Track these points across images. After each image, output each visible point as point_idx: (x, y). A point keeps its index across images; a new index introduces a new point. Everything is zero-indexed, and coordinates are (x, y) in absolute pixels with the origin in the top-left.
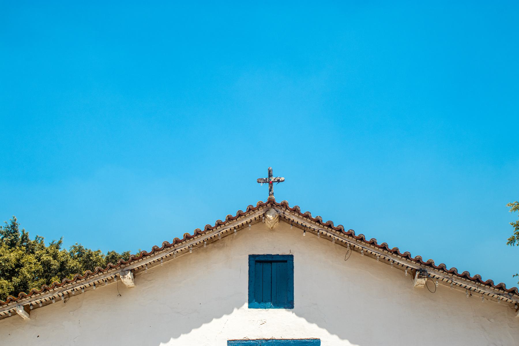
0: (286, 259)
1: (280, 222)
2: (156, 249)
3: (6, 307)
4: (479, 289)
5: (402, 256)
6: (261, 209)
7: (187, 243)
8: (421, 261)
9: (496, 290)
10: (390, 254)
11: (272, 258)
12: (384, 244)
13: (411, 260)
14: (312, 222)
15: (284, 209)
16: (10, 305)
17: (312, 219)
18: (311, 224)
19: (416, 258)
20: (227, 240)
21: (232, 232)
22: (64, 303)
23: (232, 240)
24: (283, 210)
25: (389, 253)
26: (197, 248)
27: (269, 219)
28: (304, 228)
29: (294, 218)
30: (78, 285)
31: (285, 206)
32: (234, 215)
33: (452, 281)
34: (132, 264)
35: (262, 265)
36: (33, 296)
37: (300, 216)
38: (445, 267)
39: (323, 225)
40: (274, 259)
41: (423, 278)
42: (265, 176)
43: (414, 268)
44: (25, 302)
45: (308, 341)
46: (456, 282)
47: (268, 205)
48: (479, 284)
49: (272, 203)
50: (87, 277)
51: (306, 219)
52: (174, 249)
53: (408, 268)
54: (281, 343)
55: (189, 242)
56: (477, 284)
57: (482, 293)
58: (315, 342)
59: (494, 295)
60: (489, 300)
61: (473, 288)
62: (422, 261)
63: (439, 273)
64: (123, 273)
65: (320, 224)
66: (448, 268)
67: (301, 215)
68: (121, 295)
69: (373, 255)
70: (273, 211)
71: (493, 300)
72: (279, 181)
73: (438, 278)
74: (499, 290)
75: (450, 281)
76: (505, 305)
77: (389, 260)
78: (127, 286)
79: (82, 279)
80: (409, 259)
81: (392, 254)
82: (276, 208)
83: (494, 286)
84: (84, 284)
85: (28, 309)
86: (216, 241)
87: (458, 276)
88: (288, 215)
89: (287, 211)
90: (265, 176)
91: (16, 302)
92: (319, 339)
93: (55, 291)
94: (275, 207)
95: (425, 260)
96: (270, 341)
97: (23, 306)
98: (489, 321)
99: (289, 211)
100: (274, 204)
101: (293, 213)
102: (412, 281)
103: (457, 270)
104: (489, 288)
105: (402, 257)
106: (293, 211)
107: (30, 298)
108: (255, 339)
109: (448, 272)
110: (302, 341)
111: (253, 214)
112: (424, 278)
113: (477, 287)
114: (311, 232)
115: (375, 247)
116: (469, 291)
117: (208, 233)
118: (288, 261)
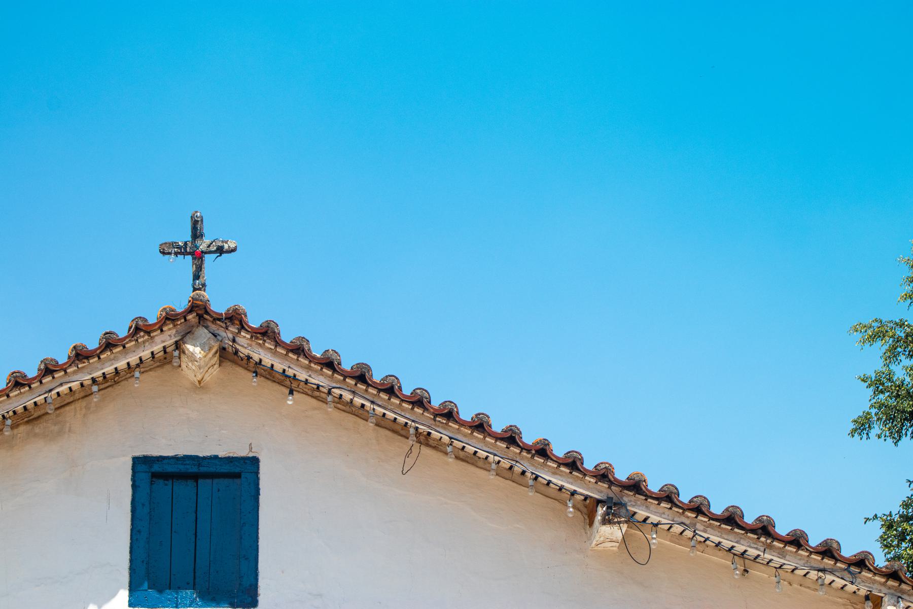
0: (237, 470)
1: (224, 364)
4: (768, 556)
5: (560, 463)
6: (170, 329)
8: (610, 477)
10: (527, 457)
12: (511, 430)
13: (585, 475)
14: (312, 365)
15: (233, 329)
17: (312, 359)
19: (598, 467)
21: (85, 392)
24: (232, 332)
25: (524, 454)
28: (290, 384)
37: (279, 350)
38: (675, 494)
39: (342, 375)
40: (203, 469)
41: (615, 523)
42: (184, 236)
46: (706, 535)
47: (190, 317)
48: (769, 541)
51: (295, 357)
56: (763, 543)
59: (808, 573)
60: (795, 586)
61: (752, 552)
62: (614, 477)
63: (661, 511)
65: (334, 370)
67: (283, 347)
69: (479, 458)
71: (805, 587)
75: (689, 533)
80: (578, 470)
82: (213, 327)
87: (711, 519)
88: (246, 346)
90: (184, 236)
94: (210, 324)
95: (621, 475)
99: (248, 336)
100: (205, 316)
101: (261, 342)
104: (796, 552)
105: (560, 465)
109: (685, 508)
111: (147, 344)
112: (619, 523)
113: (762, 549)
114: (310, 392)
115: (485, 437)
116: (741, 561)
117: (16, 396)
118: (243, 476)
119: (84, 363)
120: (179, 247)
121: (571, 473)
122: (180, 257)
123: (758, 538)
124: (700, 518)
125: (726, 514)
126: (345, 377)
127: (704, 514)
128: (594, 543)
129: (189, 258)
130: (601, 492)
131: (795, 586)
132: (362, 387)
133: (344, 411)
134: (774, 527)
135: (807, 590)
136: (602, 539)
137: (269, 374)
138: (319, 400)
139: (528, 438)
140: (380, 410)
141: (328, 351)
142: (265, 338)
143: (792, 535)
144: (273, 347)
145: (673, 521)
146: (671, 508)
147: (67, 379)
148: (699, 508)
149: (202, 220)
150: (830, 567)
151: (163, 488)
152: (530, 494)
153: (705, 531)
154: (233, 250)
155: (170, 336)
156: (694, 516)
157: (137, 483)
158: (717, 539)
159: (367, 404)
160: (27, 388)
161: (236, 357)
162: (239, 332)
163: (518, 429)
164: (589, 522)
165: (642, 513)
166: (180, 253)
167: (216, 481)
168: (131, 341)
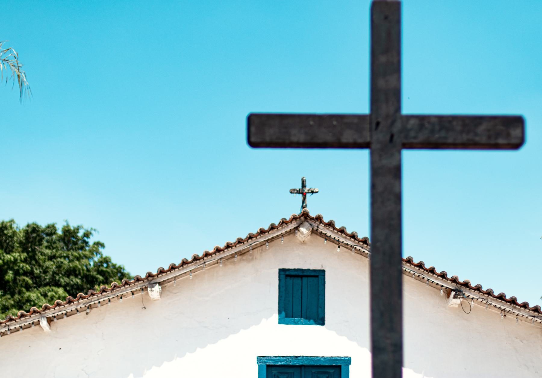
0: (317, 274)
1: (312, 234)
2: (185, 262)
3: (29, 318)
4: (514, 311)
5: (438, 275)
6: (294, 222)
7: (217, 256)
8: (457, 281)
9: (531, 313)
10: (426, 273)
11: (303, 272)
12: (421, 263)
13: (448, 280)
14: (347, 237)
15: (318, 223)
16: (33, 317)
17: (347, 235)
18: (346, 240)
19: (453, 278)
20: (256, 252)
21: (262, 244)
22: (86, 315)
23: (261, 253)
24: (317, 224)
25: (425, 272)
26: (224, 261)
27: (302, 233)
28: (338, 243)
29: (329, 232)
30: (103, 297)
31: (319, 220)
32: (266, 228)
33: (487, 302)
34: (160, 277)
35: (292, 280)
36: (57, 308)
37: (335, 231)
38: (481, 288)
39: (358, 241)
40: (305, 274)
41: (458, 298)
42: (299, 186)
43: (449, 288)
44: (48, 313)
45: (339, 358)
46: (491, 303)
47: (302, 218)
48: (515, 306)
49: (305, 215)
50: (113, 289)
51: (341, 234)
52: (203, 262)
53: (447, 289)
54: (311, 360)
55: (218, 256)
56: (512, 306)
57: (517, 315)
58: (346, 359)
59: (528, 317)
60: (523, 321)
61: (508, 309)
62: (458, 281)
63: (475, 294)
64: (151, 285)
65: (355, 239)
66: (484, 289)
67: (336, 230)
68: (145, 308)
69: (407, 272)
70: (306, 224)
71: (527, 322)
72: (312, 192)
73: (473, 298)
74: (534, 312)
75: (484, 302)
76: (539, 327)
77: (423, 278)
78: (152, 298)
79: (108, 291)
80: (445, 278)
81: (428, 273)
82: (310, 222)
83: (529, 308)
84: (109, 296)
85: (50, 321)
86: (244, 253)
87: (493, 297)
88: (322, 229)
89: (321, 224)
90: (299, 186)
91: (39, 314)
92: (350, 357)
93: (79, 303)
94: (309, 220)
95: (461, 280)
96: (300, 358)
97: (47, 318)
98: (522, 343)
99: (323, 225)
100: (307, 218)
101: (328, 228)
102: (446, 301)
103: (493, 291)
104: (524, 310)
105: (438, 276)
106: (327, 225)
107: (53, 309)
108: (285, 356)
109: (484, 293)
110: (333, 359)
111: (286, 228)
112: (460, 298)
113: (512, 308)
114: (344, 246)
115: (411, 265)
116: (504, 312)
117: (238, 246)
118: (319, 276)
119: (263, 234)
120: (297, 191)
121: (442, 279)
122: (298, 194)
123: (511, 305)
124: (490, 297)
125: (500, 296)
126: (359, 242)
127: (491, 295)
128: (449, 304)
129: (301, 195)
130: (453, 286)
131: (523, 321)
132: (365, 245)
133: (357, 253)
134: (517, 301)
135: (528, 323)
136: (452, 303)
137: (333, 241)
138: (347, 249)
139: (427, 266)
140: (363, 250)
141: (353, 232)
142: (330, 227)
143: (53, 290)
144: (332, 230)
145: (479, 297)
146: (479, 293)
147: (257, 240)
148: (489, 293)
149: (305, 181)
150: (537, 315)
151: (290, 281)
152: (427, 287)
153: (491, 302)
154: (317, 192)
155: (294, 225)
156: (487, 296)
157: (281, 278)
158: (494, 304)
159: (361, 249)
160: (242, 244)
161: (317, 232)
162: (320, 224)
163: (423, 263)
164: (448, 296)
165: (467, 294)
166: (298, 193)
167: (309, 278)
168: (280, 227)
